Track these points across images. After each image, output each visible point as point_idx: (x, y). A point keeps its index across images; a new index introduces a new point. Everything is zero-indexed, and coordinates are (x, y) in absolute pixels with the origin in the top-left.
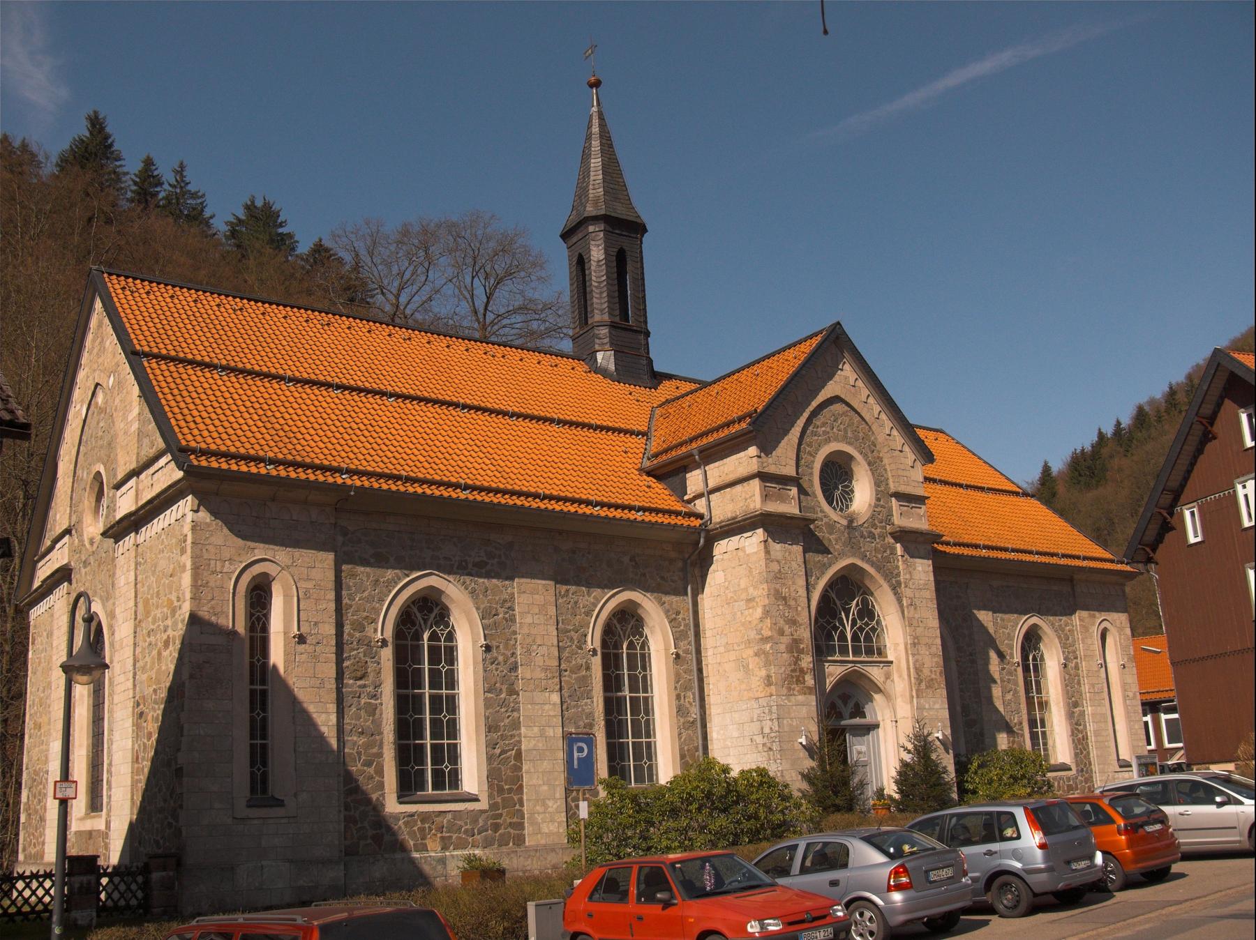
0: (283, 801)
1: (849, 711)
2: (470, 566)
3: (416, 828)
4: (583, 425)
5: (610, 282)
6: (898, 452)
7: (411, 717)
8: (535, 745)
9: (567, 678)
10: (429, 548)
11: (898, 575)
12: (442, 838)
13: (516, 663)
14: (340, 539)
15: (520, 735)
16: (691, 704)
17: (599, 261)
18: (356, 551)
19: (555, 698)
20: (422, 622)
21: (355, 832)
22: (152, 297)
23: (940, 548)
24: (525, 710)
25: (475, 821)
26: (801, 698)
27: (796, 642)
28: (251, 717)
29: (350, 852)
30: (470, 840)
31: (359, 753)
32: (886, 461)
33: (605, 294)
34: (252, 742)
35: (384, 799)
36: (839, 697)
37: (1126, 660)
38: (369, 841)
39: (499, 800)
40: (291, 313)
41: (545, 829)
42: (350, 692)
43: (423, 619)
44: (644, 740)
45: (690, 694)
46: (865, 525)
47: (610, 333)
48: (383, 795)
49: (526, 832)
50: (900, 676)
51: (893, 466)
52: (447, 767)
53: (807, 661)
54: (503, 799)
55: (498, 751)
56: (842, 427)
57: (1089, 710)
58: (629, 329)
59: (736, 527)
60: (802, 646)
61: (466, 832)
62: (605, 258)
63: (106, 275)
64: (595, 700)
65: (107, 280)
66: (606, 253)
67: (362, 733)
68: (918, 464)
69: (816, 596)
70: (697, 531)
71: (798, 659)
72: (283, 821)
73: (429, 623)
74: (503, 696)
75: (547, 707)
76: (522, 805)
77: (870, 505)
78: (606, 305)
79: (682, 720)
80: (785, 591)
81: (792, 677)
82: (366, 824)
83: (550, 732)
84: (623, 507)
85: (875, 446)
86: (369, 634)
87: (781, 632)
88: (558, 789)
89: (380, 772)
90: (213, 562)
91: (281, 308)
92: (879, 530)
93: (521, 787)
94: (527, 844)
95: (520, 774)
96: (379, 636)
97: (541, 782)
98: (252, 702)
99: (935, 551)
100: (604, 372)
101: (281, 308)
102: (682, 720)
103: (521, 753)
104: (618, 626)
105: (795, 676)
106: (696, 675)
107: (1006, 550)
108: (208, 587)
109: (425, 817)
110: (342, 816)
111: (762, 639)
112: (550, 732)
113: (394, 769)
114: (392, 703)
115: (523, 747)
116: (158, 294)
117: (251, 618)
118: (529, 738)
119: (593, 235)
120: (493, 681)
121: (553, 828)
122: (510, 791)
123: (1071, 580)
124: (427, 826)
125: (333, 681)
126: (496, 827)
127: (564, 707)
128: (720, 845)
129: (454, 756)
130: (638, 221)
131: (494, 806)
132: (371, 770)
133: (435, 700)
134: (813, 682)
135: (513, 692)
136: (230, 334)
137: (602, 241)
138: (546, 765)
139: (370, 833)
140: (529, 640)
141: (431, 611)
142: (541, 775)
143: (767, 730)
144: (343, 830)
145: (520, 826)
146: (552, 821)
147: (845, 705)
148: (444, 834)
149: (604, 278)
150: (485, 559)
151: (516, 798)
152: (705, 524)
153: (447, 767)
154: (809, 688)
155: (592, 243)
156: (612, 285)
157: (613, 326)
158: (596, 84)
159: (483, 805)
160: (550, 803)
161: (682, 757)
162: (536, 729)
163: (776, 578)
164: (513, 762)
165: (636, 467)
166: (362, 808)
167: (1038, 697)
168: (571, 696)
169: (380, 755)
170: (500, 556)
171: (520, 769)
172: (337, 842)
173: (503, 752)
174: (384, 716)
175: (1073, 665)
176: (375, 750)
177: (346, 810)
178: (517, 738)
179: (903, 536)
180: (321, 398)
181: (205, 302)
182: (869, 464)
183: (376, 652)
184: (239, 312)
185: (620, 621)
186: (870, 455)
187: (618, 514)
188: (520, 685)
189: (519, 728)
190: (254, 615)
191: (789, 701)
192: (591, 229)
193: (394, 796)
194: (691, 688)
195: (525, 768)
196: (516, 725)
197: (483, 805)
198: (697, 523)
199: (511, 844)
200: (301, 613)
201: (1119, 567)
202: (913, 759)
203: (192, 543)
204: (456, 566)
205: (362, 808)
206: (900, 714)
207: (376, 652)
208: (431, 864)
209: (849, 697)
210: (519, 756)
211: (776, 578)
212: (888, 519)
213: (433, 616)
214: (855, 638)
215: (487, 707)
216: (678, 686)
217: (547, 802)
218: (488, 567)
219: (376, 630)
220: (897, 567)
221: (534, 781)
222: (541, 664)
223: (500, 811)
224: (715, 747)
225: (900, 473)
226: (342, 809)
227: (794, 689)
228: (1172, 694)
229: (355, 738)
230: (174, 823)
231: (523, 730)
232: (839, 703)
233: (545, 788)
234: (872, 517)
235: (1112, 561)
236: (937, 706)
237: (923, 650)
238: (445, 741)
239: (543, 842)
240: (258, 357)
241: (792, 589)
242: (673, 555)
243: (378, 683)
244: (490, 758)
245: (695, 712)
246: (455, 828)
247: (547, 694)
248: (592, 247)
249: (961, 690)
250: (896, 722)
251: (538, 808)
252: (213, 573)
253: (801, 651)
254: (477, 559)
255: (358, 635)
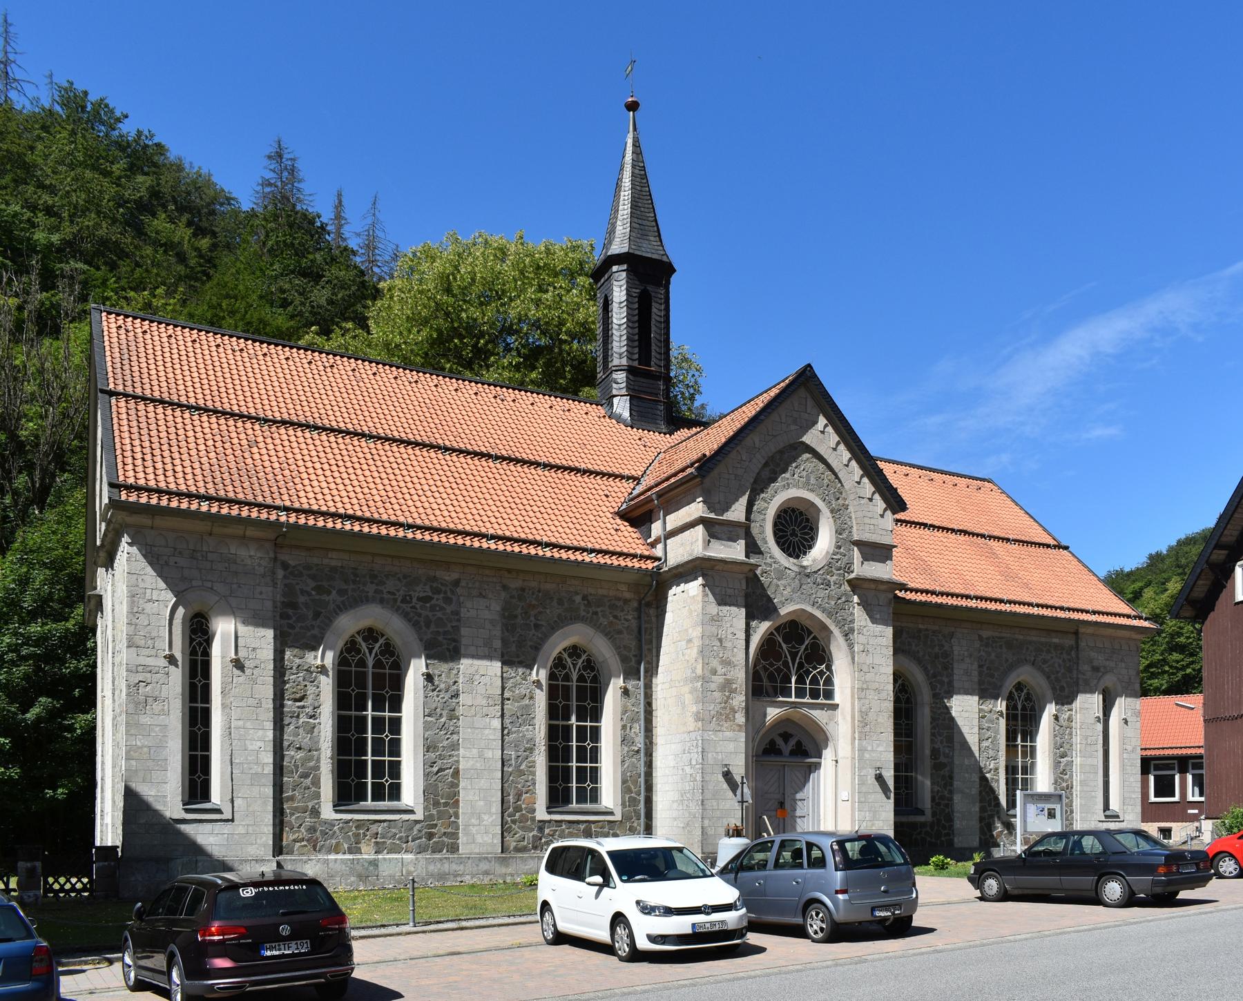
1: (790, 748)
2: (414, 600)
3: (350, 834)
4: (571, 469)
5: (630, 324)
6: (866, 501)
7: (560, 743)
9: (509, 707)
11: (852, 621)
12: (377, 843)
13: (458, 691)
15: (458, 756)
16: (637, 735)
17: (621, 303)
18: (298, 584)
19: (497, 723)
20: (367, 651)
22: (313, 367)
23: (901, 594)
24: (464, 733)
26: (728, 734)
27: (728, 683)
30: (404, 845)
31: (297, 767)
32: (851, 509)
33: (625, 337)
35: (320, 807)
36: (780, 735)
37: (1129, 714)
39: (434, 812)
40: (442, 382)
41: (479, 839)
42: (290, 712)
44: (588, 765)
45: (636, 725)
46: (821, 572)
47: (627, 377)
48: (319, 803)
49: (460, 841)
50: (844, 718)
51: (860, 514)
52: (387, 781)
53: (739, 700)
55: (435, 769)
56: (804, 473)
57: (1078, 761)
58: (649, 375)
59: (685, 572)
60: (734, 686)
61: (400, 839)
62: (627, 300)
63: (104, 314)
64: (537, 727)
65: (104, 318)
66: (628, 294)
67: (300, 748)
68: (889, 513)
69: (755, 640)
70: (656, 573)
73: (374, 652)
74: (443, 720)
75: (487, 732)
76: (457, 816)
77: (828, 552)
78: (625, 348)
79: (626, 749)
80: (722, 634)
81: (721, 714)
83: (489, 754)
84: (1082, 611)
85: (841, 493)
86: (308, 661)
87: (714, 672)
89: (316, 783)
90: (148, 591)
91: (473, 384)
92: (835, 578)
93: (457, 801)
94: (460, 851)
96: (319, 662)
97: (477, 798)
99: (896, 597)
100: (619, 419)
101: (473, 384)
102: (626, 749)
103: (458, 772)
104: (568, 660)
105: (726, 714)
106: (642, 706)
107: (1001, 601)
109: (360, 825)
111: (695, 678)
112: (489, 754)
113: (331, 781)
114: (330, 722)
115: (461, 767)
116: (383, 375)
117: (191, 643)
118: (467, 759)
119: (617, 274)
120: (433, 706)
121: (488, 839)
122: (446, 804)
123: (1076, 633)
124: (362, 832)
125: (271, 701)
126: (430, 836)
127: (506, 732)
129: (595, 774)
130: (665, 259)
131: (428, 818)
132: (308, 781)
133: (378, 724)
134: (743, 720)
135: (453, 716)
136: (404, 405)
137: (624, 281)
138: (483, 783)
142: (477, 792)
143: (694, 762)
145: (455, 835)
147: (786, 743)
149: (625, 320)
150: (430, 594)
151: (451, 811)
152: (659, 568)
153: (588, 785)
154: (740, 726)
155: (615, 283)
156: (631, 328)
157: (630, 370)
158: (633, 107)
159: (419, 816)
160: (486, 817)
161: (624, 782)
162: (475, 751)
163: (713, 619)
165: (612, 511)
167: (1022, 746)
169: (317, 768)
171: (457, 785)
173: (440, 770)
174: (322, 734)
175: (1066, 717)
176: (312, 764)
178: (455, 758)
179: (857, 585)
180: (508, 473)
181: (341, 367)
182: (832, 512)
183: (316, 677)
184: (414, 385)
186: (833, 502)
187: (615, 561)
188: (460, 711)
189: (458, 750)
192: (615, 268)
193: (330, 805)
194: (638, 720)
195: (462, 784)
196: (455, 746)
197: (419, 816)
198: (650, 565)
200: (240, 640)
201: (1136, 623)
204: (399, 600)
206: (841, 754)
207: (316, 677)
209: (791, 736)
210: (456, 773)
211: (713, 619)
212: (848, 568)
215: (426, 729)
216: (625, 718)
217: (483, 816)
218: (434, 602)
219: (316, 657)
220: (852, 614)
221: (471, 798)
222: (484, 692)
224: (659, 774)
225: (867, 521)
227: (722, 726)
228: (1202, 751)
229: (292, 753)
231: (462, 751)
232: (780, 742)
233: (482, 803)
234: (829, 564)
235: (1129, 616)
236: (881, 749)
237: (871, 695)
238: (387, 758)
239: (477, 851)
240: (361, 418)
241: (729, 632)
242: (627, 595)
243: (316, 705)
244: (427, 775)
245: (640, 743)
246: (390, 835)
247: (488, 720)
248: (615, 288)
249: (933, 735)
250: (837, 761)
252: (149, 601)
253: (734, 691)
254: (422, 594)
255: (298, 661)
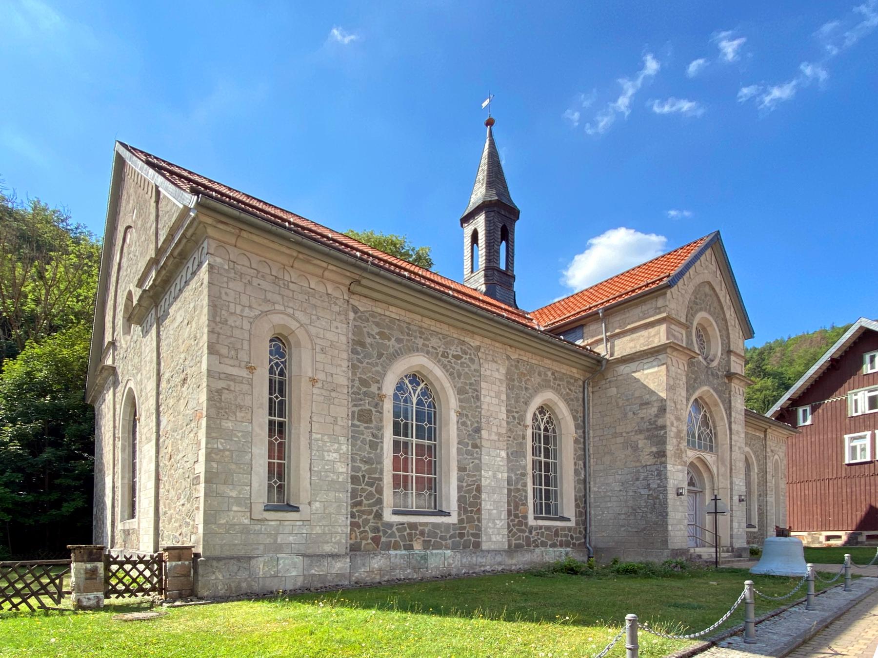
0: (298, 508)
2: (450, 356)
3: (405, 533)
8: (489, 483)
10: (421, 338)
14: (352, 315)
15: (480, 476)
21: (358, 534)
25: (447, 531)
26: (680, 467)
28: (269, 441)
29: (354, 549)
31: (364, 476)
34: (270, 460)
35: (382, 510)
38: (370, 541)
39: (464, 517)
43: (413, 389)
54: (467, 517)
71: (679, 443)
72: (298, 523)
75: (498, 459)
82: (367, 528)
88: (503, 513)
90: (232, 305)
95: (479, 501)
98: (270, 431)
104: (539, 415)
108: (227, 324)
109: (413, 526)
110: (349, 522)
118: (487, 478)
121: (499, 538)
128: (430, 527)
131: (461, 521)
139: (371, 535)
140: (489, 414)
141: (419, 385)
144: (349, 532)
146: (499, 534)
148: (426, 539)
150: (460, 354)
151: (475, 517)
160: (498, 522)
162: (490, 473)
164: (474, 493)
166: (365, 517)
168: (515, 454)
170: (470, 355)
171: (480, 498)
172: (344, 541)
176: (377, 476)
177: (351, 517)
185: (540, 413)
190: (273, 361)
191: (674, 468)
199: (471, 547)
202: (33, 496)
203: (209, 283)
205: (365, 517)
208: (417, 559)
210: (479, 489)
213: (420, 388)
214: (699, 436)
217: (496, 521)
218: (463, 360)
221: (488, 507)
223: (465, 525)
226: (349, 516)
230: (191, 523)
233: (495, 511)
239: (492, 547)
251: (490, 524)
254: (455, 353)
